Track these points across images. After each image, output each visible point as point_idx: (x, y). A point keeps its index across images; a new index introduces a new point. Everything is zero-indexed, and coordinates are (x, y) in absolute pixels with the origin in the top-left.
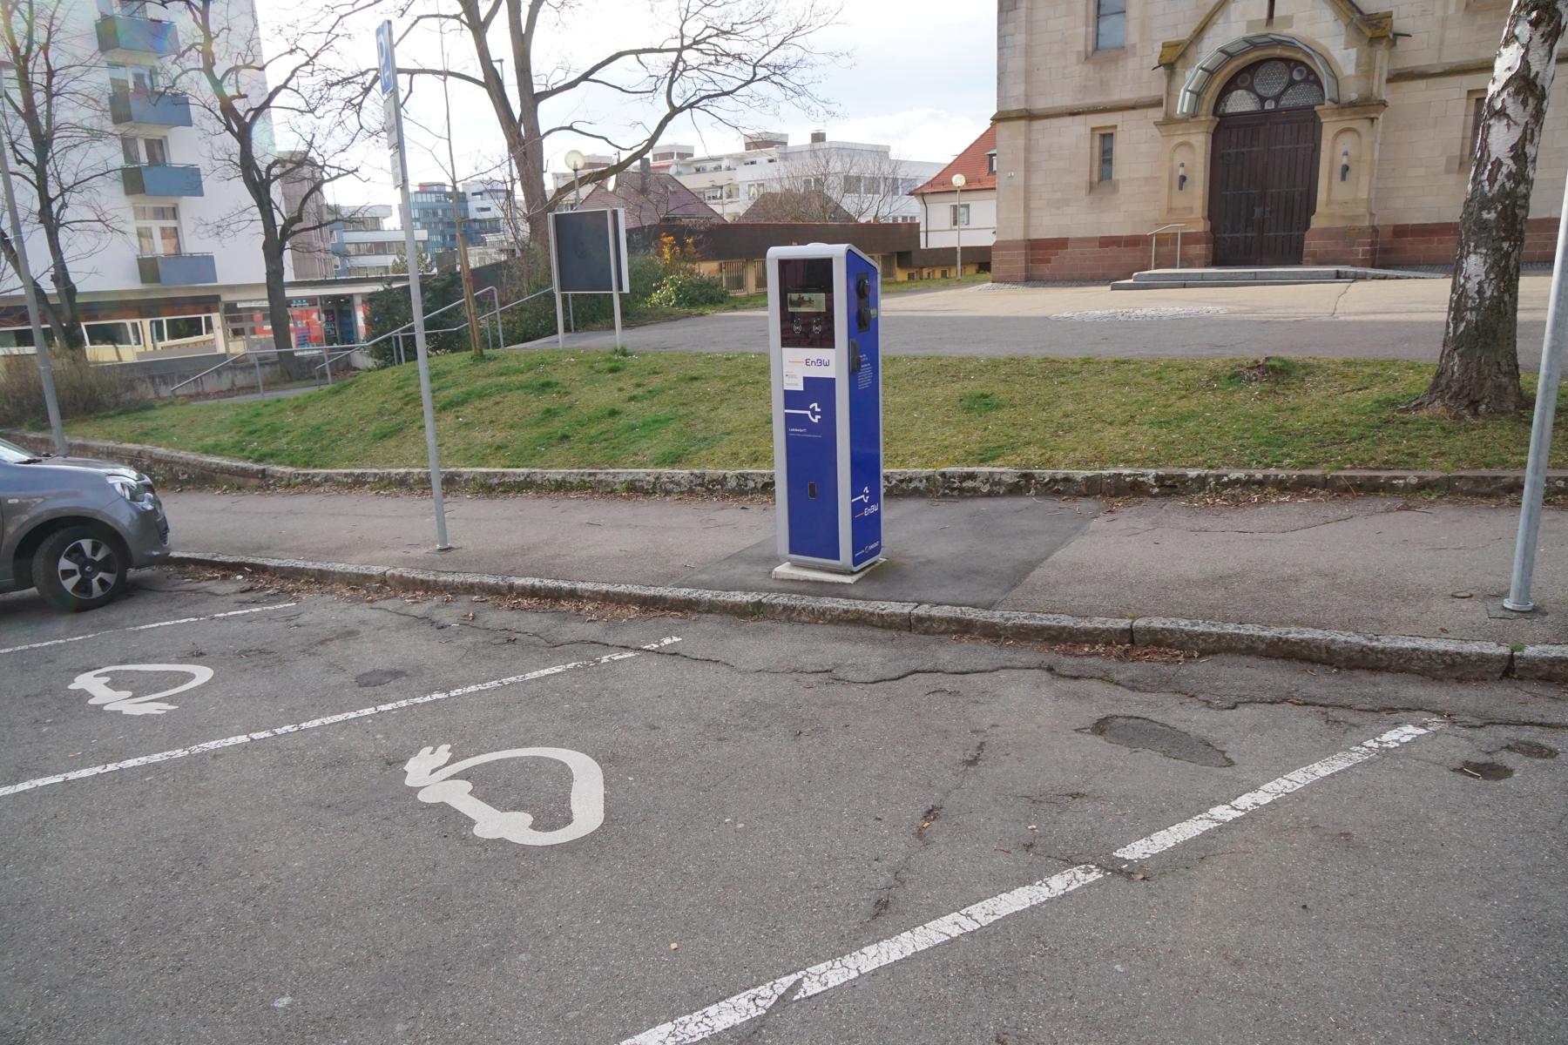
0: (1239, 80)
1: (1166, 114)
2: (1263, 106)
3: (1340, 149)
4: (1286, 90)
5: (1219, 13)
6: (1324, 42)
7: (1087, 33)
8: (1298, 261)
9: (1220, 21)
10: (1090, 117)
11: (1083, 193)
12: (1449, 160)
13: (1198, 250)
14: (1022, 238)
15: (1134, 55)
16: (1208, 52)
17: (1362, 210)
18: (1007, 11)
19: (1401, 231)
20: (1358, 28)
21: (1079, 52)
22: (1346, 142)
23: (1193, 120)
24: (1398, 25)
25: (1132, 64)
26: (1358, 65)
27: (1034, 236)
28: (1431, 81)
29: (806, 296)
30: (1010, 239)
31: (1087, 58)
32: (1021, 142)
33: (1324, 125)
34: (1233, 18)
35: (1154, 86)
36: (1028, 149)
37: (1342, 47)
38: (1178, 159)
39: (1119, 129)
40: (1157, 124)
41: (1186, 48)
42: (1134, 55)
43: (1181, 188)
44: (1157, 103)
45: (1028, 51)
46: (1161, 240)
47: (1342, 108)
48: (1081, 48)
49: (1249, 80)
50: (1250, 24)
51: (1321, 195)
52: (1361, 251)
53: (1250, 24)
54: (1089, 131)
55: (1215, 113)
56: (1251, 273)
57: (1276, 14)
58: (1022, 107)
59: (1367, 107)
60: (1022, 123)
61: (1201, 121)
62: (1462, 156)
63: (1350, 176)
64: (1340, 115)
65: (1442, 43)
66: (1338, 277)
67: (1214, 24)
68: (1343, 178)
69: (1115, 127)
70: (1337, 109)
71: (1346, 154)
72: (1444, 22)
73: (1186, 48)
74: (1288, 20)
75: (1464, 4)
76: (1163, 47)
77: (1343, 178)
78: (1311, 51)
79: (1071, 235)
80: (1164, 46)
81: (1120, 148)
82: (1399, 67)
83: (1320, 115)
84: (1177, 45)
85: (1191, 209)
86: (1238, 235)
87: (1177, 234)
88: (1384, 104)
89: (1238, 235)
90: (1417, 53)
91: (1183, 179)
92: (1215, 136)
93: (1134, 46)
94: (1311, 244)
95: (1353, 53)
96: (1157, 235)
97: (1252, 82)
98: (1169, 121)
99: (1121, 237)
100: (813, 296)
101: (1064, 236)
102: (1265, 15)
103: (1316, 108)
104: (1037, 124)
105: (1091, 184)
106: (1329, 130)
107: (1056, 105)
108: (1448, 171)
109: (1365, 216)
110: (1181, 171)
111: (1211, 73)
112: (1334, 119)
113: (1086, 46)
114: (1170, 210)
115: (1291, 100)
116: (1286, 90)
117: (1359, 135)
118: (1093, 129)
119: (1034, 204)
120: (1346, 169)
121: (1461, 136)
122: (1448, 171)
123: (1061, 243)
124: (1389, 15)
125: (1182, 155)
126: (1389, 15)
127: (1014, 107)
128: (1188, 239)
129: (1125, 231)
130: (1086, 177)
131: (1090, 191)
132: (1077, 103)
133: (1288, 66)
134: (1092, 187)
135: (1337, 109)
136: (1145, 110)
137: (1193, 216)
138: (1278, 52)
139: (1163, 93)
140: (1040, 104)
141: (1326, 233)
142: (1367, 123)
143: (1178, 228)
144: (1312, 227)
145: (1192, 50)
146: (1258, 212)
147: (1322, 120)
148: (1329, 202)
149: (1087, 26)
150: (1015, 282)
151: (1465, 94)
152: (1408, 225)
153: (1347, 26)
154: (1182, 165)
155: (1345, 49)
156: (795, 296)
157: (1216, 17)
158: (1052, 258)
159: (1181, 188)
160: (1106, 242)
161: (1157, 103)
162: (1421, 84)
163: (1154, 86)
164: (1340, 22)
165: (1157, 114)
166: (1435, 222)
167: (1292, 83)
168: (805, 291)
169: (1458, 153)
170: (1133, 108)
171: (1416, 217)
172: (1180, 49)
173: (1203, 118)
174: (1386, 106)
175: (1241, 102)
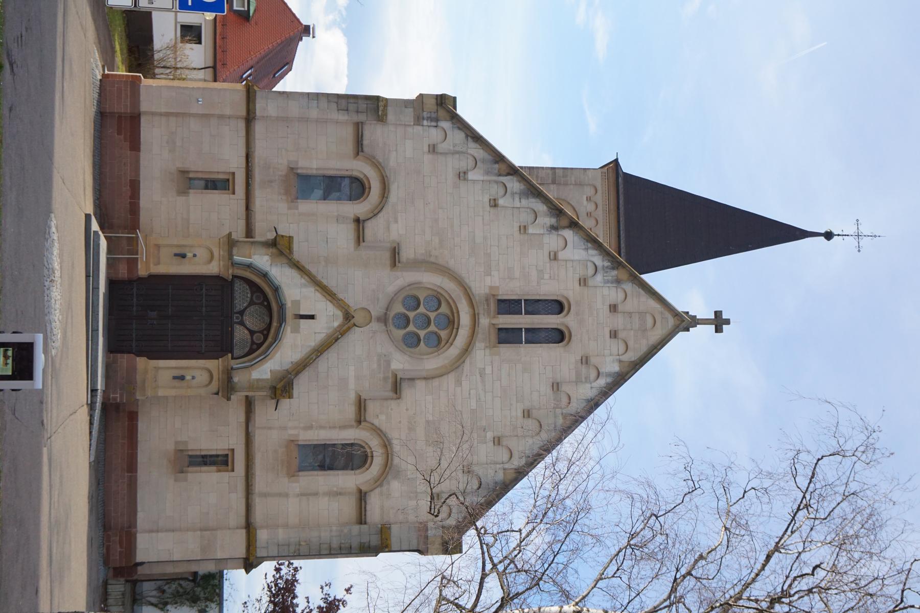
0: (259, 294)
1: (237, 241)
2: (237, 313)
3: (197, 373)
4: (248, 329)
5: (308, 279)
6: (278, 355)
7: (311, 169)
8: (113, 348)
9: (303, 281)
10: (243, 171)
11: (179, 165)
12: (186, 443)
13: (123, 272)
14: (141, 110)
15: (289, 208)
16: (282, 275)
17: (149, 393)
18: (337, 103)
19: (133, 417)
20: (284, 378)
21: (297, 162)
22: (202, 377)
23: (230, 264)
24: (285, 403)
25: (282, 207)
26: (258, 380)
27: (143, 120)
28: (244, 425)
29: (10, 361)
30: (141, 98)
31: (292, 169)
32: (228, 111)
33: (216, 361)
34: (304, 290)
35: (263, 232)
36: (221, 117)
37: (272, 369)
38: (199, 252)
39: (232, 196)
40: (230, 234)
41: (286, 256)
42: (289, 208)
43: (176, 255)
44: (249, 232)
45: (304, 120)
46: (133, 242)
47: (228, 373)
48: (300, 165)
49: (258, 302)
50: (297, 303)
51: (162, 363)
52: (117, 396)
53: (297, 303)
54: (232, 170)
55: (234, 277)
56: (98, 326)
57: (302, 321)
58: (258, 113)
59: (227, 388)
60: (243, 113)
61: (228, 271)
62: (188, 450)
63: (176, 383)
64: (223, 371)
65: (270, 428)
66: (92, 391)
67: (302, 277)
68: (175, 378)
69: (234, 193)
70: (228, 370)
71: (193, 378)
72: (284, 428)
73: (286, 256)
74: (296, 330)
75: (292, 439)
76: (290, 237)
77: (175, 378)
78: (266, 356)
79: (143, 155)
80: (290, 238)
81: (216, 197)
82: (256, 402)
83: (223, 358)
84: (290, 249)
85: (158, 263)
86: (135, 300)
87: (137, 254)
88: (229, 399)
89: (135, 300)
90: (264, 413)
91: (183, 256)
92: (217, 278)
93: (297, 208)
94: (123, 360)
95: (268, 376)
96: (138, 237)
97: (255, 304)
98: (231, 243)
99: (139, 199)
100: (10, 366)
101: (142, 147)
102: (302, 313)
103: (230, 355)
104: (242, 125)
105: (188, 172)
106: (213, 364)
107: (257, 141)
108: (177, 443)
109: (145, 396)
110: (189, 255)
111: (265, 276)
112: (220, 367)
113: (302, 168)
114: (158, 247)
115: (240, 334)
116: (248, 329)
117: (207, 386)
118: (233, 174)
119: (173, 120)
120: (182, 378)
121: (202, 448)
122: (177, 443)
123: (135, 144)
124: (291, 397)
125: (202, 254)
126: (291, 397)
127: (258, 106)
128: (132, 263)
129: (144, 202)
130: (193, 168)
131: (180, 171)
132: (256, 160)
133: (265, 329)
134: (183, 172)
135: (228, 370)
136: (244, 217)
137: (152, 265)
138: (275, 324)
139: (258, 238)
140: (259, 128)
141: (133, 369)
142: (215, 390)
143: (142, 257)
144: (138, 359)
145: (285, 260)
146: (154, 314)
147: (220, 359)
148: (157, 369)
149: (317, 169)
150: (100, 102)
151: (231, 447)
152: (137, 421)
153: (287, 370)
154: (195, 256)
155: (271, 370)
156: (10, 353)
157: (306, 278)
158: (122, 137)
159: (176, 255)
160: (135, 186)
161: (249, 232)
162: (242, 419)
163: (263, 232)
164: (290, 365)
165: (239, 233)
166: (139, 439)
167: (252, 333)
168: (13, 360)
169: (189, 448)
170: (248, 208)
171: (142, 425)
172: (286, 251)
173: (230, 271)
174: (228, 400)
175: (240, 290)
